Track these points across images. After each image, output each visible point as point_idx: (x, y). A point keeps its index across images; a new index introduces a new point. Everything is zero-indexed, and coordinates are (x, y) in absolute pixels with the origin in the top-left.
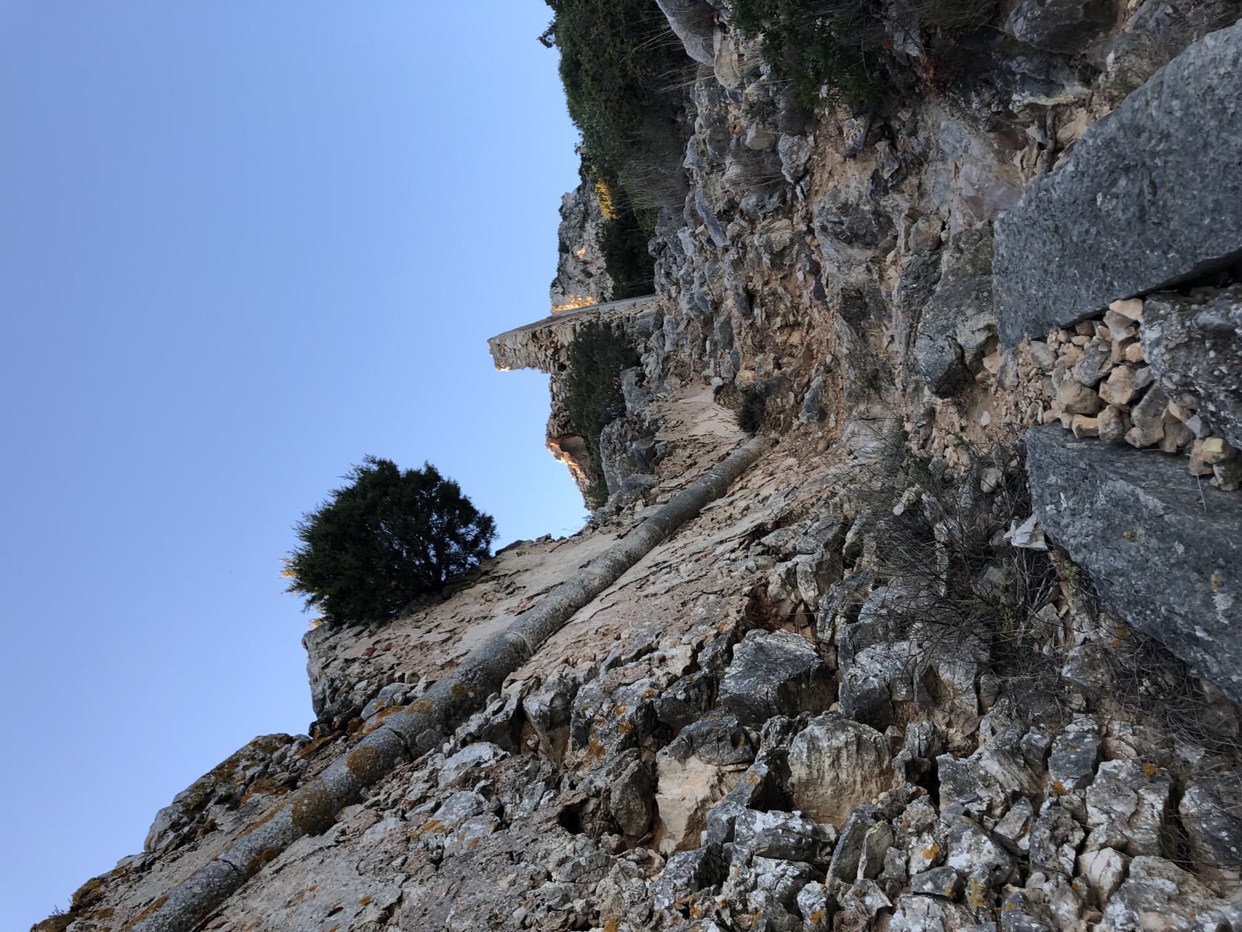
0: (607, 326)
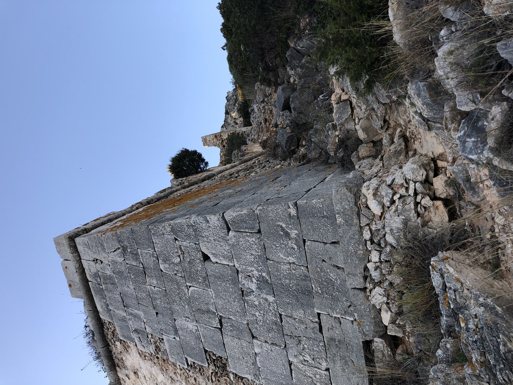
0: (238, 134)
